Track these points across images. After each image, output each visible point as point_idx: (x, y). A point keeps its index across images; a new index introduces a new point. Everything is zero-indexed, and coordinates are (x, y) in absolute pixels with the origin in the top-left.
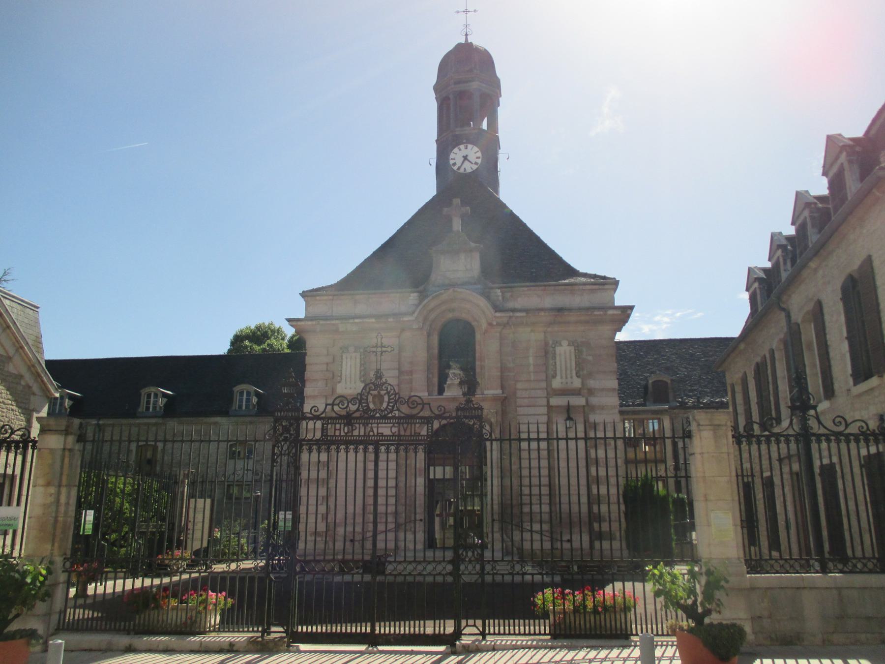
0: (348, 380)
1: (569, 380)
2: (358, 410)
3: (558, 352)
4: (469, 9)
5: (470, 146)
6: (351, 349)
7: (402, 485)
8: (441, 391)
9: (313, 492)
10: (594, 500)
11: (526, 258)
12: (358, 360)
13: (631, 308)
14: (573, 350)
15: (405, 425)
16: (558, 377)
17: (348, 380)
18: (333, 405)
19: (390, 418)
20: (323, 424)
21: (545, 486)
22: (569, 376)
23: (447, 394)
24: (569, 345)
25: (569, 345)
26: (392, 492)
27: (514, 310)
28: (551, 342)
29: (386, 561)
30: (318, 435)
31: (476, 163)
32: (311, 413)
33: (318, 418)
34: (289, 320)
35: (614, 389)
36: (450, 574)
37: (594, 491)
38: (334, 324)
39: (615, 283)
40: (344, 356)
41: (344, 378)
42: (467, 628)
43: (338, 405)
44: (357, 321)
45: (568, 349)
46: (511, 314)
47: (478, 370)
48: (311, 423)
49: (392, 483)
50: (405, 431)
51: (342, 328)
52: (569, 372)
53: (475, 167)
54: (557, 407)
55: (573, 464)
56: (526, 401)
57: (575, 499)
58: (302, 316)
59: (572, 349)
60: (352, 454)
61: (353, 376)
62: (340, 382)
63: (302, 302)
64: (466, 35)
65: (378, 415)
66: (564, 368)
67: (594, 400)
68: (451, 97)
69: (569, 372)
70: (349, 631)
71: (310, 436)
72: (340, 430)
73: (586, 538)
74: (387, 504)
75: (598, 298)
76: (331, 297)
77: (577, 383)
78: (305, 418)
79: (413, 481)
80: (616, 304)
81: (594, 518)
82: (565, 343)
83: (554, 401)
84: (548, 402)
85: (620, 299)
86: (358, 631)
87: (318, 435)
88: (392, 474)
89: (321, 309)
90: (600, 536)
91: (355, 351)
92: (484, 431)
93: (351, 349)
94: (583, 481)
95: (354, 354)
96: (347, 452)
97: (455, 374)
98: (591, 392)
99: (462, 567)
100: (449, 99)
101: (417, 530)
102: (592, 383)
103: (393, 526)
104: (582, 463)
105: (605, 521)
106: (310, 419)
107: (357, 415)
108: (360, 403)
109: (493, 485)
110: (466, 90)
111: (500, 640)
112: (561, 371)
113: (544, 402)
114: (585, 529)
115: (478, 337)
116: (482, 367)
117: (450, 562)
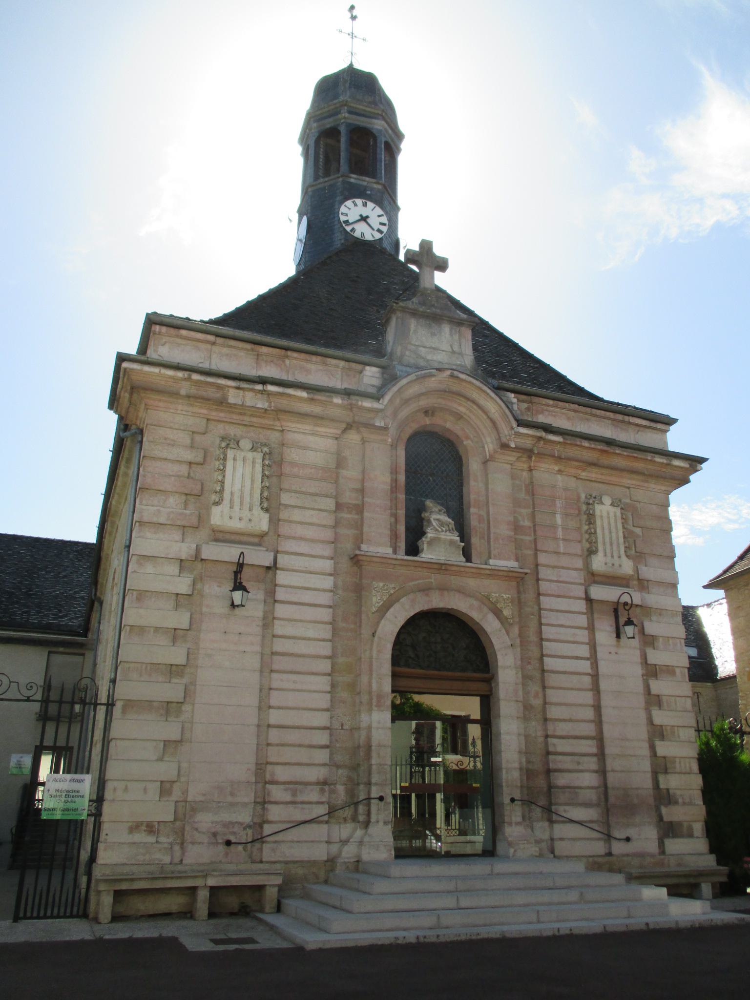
0: (237, 501)
3: (598, 513)
6: (246, 444)
8: (413, 549)
10: (661, 767)
12: (258, 468)
13: (702, 460)
14: (619, 514)
16: (600, 554)
17: (237, 501)
22: (616, 554)
23: (427, 555)
24: (612, 505)
25: (612, 505)
27: (548, 429)
28: (583, 496)
31: (379, 231)
38: (220, 387)
39: (669, 421)
40: (230, 453)
41: (227, 495)
44: (271, 388)
45: (612, 510)
46: (543, 434)
51: (233, 397)
52: (615, 547)
53: (378, 236)
54: (602, 602)
56: (554, 586)
57: (633, 770)
59: (618, 511)
61: (247, 499)
62: (217, 503)
66: (607, 540)
68: (342, 129)
74: (305, 763)
75: (647, 439)
76: (211, 338)
77: (627, 567)
81: (663, 797)
82: (607, 500)
83: (599, 592)
84: (586, 593)
91: (253, 449)
93: (246, 444)
95: (250, 455)
97: (437, 519)
100: (339, 132)
109: (510, 731)
110: (351, 136)
113: (580, 591)
115: (473, 466)
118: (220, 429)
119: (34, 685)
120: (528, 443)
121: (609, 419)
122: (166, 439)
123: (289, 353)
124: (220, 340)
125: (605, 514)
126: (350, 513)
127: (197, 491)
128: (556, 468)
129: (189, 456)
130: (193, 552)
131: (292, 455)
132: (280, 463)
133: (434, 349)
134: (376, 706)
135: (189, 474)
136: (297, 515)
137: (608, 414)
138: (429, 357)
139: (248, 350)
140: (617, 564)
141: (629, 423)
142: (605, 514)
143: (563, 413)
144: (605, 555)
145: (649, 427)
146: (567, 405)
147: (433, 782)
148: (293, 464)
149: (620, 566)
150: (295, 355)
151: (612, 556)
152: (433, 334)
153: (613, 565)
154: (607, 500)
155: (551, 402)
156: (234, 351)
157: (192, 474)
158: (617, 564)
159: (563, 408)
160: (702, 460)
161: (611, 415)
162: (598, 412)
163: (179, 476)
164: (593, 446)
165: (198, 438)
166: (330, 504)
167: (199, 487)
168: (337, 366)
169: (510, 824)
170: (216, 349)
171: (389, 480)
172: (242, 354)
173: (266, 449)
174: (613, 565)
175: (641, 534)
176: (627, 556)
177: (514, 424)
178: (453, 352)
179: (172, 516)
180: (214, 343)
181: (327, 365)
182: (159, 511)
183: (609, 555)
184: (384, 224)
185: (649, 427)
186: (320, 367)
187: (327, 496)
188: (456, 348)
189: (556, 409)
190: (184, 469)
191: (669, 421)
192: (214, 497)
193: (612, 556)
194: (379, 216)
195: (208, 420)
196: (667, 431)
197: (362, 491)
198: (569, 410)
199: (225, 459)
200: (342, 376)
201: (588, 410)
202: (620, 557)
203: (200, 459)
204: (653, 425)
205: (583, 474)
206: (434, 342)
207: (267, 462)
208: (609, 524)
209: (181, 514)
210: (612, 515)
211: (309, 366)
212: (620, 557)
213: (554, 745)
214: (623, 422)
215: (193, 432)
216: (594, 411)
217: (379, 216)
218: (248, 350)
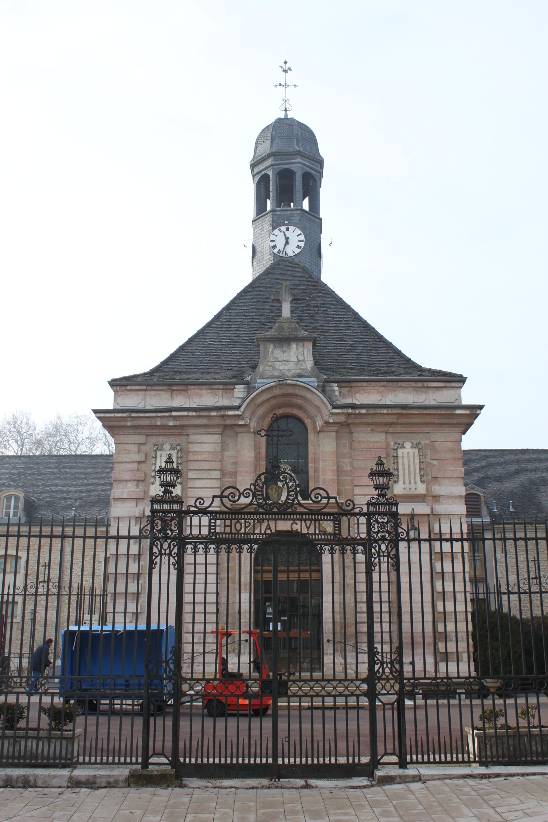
1: (413, 486)
2: (251, 504)
3: (400, 454)
4: (288, 84)
5: (292, 228)
7: (223, 600)
9: (120, 608)
11: (355, 350)
13: (481, 407)
15: (308, 523)
18: (221, 497)
19: (290, 514)
20: (210, 520)
21: (385, 602)
22: (413, 482)
24: (412, 447)
25: (412, 447)
26: (212, 608)
27: (354, 407)
29: (289, 680)
30: (205, 531)
32: (196, 506)
33: (203, 512)
34: (96, 412)
35: (461, 496)
36: (365, 694)
37: (440, 607)
39: (461, 380)
40: (159, 453)
42: (385, 757)
43: (228, 497)
45: (411, 451)
46: (350, 411)
47: (311, 472)
48: (196, 520)
49: (212, 598)
50: (308, 528)
52: (412, 476)
55: (416, 579)
58: (110, 407)
60: (224, 555)
62: (153, 483)
63: (110, 392)
64: (286, 110)
65: (275, 510)
67: (440, 508)
69: (412, 476)
70: (315, 762)
71: (195, 532)
72: (230, 526)
73: (430, 660)
75: (442, 397)
76: (144, 387)
77: (421, 489)
78: (188, 512)
79: (237, 597)
80: (463, 403)
82: (408, 445)
85: (468, 396)
86: (315, 762)
87: (205, 531)
88: (212, 588)
89: (133, 401)
90: (446, 657)
92: (400, 530)
94: (427, 597)
96: (229, 552)
98: (436, 498)
99: (379, 686)
101: (242, 651)
102: (437, 490)
103: (214, 646)
104: (427, 577)
105: (451, 640)
106: (195, 513)
107: (251, 509)
108: (254, 496)
111: (425, 771)
112: (404, 475)
114: (430, 650)
116: (316, 470)
117: (364, 681)
118: (154, 440)
119: (351, 503)
120: (342, 419)
121: (412, 387)
122: (125, 450)
123: (189, 387)
124: (149, 388)
125: (406, 455)
126: (230, 478)
127: (142, 478)
128: (369, 429)
129: (137, 458)
130: (142, 512)
131: (194, 448)
132: (188, 453)
133: (286, 361)
134: (244, 590)
135: (138, 468)
136: (198, 484)
137: (410, 384)
138: (281, 368)
139: (166, 390)
140: (413, 488)
141: (428, 387)
142: (406, 455)
143: (375, 390)
144: (404, 483)
145: (445, 387)
146: (378, 384)
147: (537, 612)
148: (195, 453)
149: (416, 489)
150: (193, 387)
151: (410, 483)
152: (284, 352)
153: (410, 489)
154: (408, 445)
155: (365, 384)
156: (158, 392)
157: (140, 468)
158: (413, 488)
159: (375, 386)
160: (481, 407)
161: (414, 384)
162: (403, 384)
163: (132, 470)
164: (390, 412)
165: (142, 447)
166: (217, 474)
167: (143, 475)
168: (219, 389)
169: (327, 654)
170: (148, 393)
171: (253, 455)
172: (162, 393)
173: (178, 448)
174: (410, 489)
175: (437, 464)
176: (421, 482)
177: (330, 407)
178: (299, 361)
179: (130, 493)
180: (146, 390)
181: (212, 389)
182: (123, 492)
183: (407, 482)
184: (302, 241)
185: (445, 387)
186: (209, 391)
187: (215, 470)
188: (300, 358)
189: (370, 388)
190: (135, 465)
191: (461, 380)
192: (152, 480)
193: (410, 483)
194: (298, 236)
195: (147, 435)
196: (461, 387)
197: (236, 463)
198: (380, 386)
199: (156, 457)
200: (222, 394)
201: (395, 384)
202: (415, 483)
203: (143, 459)
204: (447, 384)
205: (391, 429)
206: (285, 356)
207: (179, 455)
208: (409, 461)
209: (135, 492)
210: (411, 454)
211: (201, 392)
212: (415, 483)
213: (361, 608)
214: (423, 387)
215: (139, 444)
216: (399, 384)
217: (298, 236)
218: (166, 390)
